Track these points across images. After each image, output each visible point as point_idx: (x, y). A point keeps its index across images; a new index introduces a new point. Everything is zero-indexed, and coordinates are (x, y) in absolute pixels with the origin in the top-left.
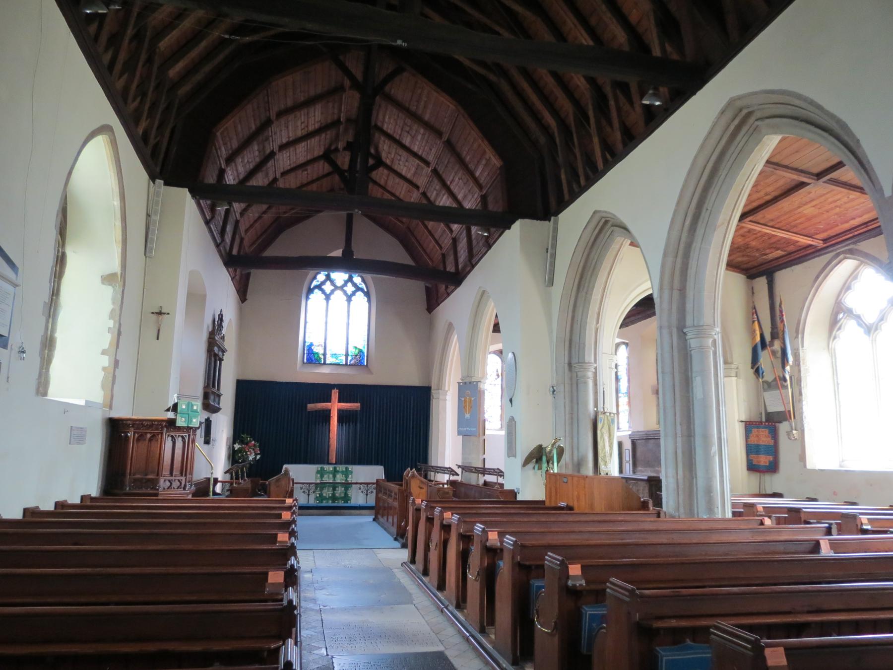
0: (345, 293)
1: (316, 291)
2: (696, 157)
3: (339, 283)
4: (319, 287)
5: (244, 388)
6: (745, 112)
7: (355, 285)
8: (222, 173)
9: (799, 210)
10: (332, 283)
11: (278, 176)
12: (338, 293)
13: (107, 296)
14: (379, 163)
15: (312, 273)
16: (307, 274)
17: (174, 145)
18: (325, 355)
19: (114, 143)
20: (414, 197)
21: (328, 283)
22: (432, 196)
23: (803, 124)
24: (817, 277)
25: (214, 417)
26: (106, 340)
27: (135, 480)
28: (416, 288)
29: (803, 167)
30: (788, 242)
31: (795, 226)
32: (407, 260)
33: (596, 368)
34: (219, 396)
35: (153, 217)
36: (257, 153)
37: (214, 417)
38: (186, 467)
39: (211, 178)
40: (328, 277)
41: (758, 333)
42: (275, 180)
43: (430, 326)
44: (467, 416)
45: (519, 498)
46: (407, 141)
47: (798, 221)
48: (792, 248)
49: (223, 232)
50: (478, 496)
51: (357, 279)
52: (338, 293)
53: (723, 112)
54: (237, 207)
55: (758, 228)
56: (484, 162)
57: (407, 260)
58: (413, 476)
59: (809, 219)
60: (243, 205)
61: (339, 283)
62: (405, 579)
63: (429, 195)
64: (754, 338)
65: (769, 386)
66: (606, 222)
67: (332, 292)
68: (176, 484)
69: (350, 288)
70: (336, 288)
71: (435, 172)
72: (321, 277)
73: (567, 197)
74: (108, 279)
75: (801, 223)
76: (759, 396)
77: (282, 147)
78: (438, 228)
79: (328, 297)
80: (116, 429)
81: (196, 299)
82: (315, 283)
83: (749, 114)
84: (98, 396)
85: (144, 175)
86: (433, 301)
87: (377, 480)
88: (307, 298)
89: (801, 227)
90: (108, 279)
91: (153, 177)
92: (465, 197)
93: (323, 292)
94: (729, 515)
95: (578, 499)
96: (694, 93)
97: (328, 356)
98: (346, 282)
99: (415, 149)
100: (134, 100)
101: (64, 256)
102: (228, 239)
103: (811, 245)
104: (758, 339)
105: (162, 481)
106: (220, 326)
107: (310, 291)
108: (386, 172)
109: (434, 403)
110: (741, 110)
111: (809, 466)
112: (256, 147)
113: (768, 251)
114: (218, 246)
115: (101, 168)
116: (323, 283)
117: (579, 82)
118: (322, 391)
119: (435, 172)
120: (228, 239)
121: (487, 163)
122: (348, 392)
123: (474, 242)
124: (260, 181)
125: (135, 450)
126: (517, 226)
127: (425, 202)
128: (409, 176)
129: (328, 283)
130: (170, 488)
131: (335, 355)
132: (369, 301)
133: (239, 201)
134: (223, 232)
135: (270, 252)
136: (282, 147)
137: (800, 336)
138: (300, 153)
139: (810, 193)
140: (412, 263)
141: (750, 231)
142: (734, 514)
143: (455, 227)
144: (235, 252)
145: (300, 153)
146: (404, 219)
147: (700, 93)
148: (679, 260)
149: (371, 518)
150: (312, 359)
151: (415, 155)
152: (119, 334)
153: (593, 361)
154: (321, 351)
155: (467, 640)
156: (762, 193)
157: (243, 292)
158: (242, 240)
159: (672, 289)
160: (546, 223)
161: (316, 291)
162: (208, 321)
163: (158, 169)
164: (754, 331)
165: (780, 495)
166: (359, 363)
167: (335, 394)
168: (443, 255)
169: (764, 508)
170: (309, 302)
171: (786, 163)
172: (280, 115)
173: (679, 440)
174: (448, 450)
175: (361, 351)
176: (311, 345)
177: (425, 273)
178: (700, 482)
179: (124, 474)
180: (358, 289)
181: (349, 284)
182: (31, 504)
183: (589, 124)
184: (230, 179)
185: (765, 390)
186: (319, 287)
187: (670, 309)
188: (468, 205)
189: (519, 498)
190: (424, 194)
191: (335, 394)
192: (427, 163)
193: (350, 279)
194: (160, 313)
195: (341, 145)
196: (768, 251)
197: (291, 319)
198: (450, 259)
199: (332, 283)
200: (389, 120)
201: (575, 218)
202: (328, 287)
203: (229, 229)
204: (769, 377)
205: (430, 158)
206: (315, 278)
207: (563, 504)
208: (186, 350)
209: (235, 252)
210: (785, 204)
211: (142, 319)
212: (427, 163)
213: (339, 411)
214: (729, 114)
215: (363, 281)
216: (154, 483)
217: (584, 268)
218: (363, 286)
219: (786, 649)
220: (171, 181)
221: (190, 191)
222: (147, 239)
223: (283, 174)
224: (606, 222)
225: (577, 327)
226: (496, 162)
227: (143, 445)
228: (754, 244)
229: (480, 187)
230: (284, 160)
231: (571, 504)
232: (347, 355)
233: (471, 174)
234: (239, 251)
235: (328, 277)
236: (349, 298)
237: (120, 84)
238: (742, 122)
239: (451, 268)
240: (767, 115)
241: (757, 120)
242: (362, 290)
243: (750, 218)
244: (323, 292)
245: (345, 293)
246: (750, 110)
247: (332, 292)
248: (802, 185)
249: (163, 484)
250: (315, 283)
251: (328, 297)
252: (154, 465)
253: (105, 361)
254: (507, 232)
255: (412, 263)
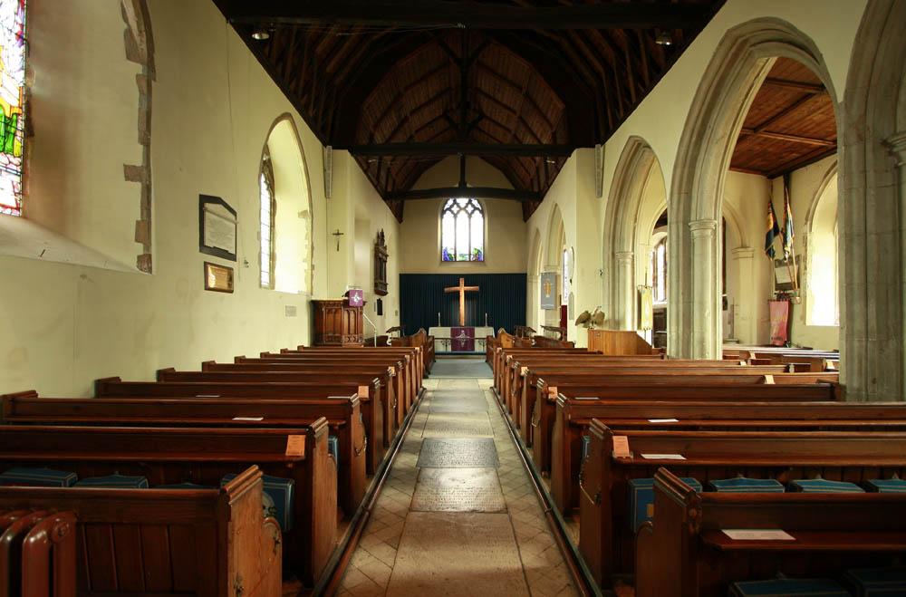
0: (467, 212)
1: (448, 212)
2: (700, 84)
3: (463, 205)
4: (449, 209)
5: (405, 280)
6: (740, 41)
7: (473, 206)
8: (372, 137)
9: (809, 118)
10: (458, 206)
11: (413, 133)
12: (463, 212)
13: (303, 225)
14: (482, 116)
15: (444, 199)
16: (440, 201)
17: (334, 123)
18: (455, 255)
19: (293, 124)
20: (508, 140)
21: (455, 206)
22: (520, 136)
23: (786, 45)
24: (828, 173)
25: (383, 298)
26: (306, 252)
27: (329, 337)
28: (515, 206)
29: (807, 81)
30: (802, 145)
31: (806, 132)
32: (510, 187)
33: (633, 256)
34: (386, 285)
35: (327, 172)
36: (395, 119)
37: (383, 298)
38: (358, 328)
39: (365, 142)
40: (455, 202)
41: (772, 222)
42: (411, 137)
43: (527, 231)
44: (548, 296)
45: (576, 346)
46: (499, 97)
47: (809, 127)
48: (805, 150)
49: (378, 179)
50: (556, 345)
51: (475, 202)
52: (463, 212)
53: (721, 44)
54: (388, 159)
55: (771, 137)
56: (552, 106)
57: (510, 187)
58: (503, 333)
59: (818, 125)
60: (391, 157)
61: (463, 205)
62: (489, 397)
63: (518, 135)
64: (768, 223)
65: (780, 263)
66: (639, 144)
67: (458, 212)
68: (352, 339)
69: (470, 209)
70: (461, 209)
71: (520, 118)
72: (450, 202)
73: (611, 127)
74: (303, 214)
75: (813, 128)
76: (770, 271)
77: (412, 113)
78: (526, 160)
79: (455, 216)
80: (316, 307)
81: (359, 224)
82: (447, 207)
83: (746, 41)
84: (304, 288)
85: (319, 143)
86: (527, 213)
87: (488, 337)
88: (442, 217)
89: (812, 131)
90: (303, 214)
91: (325, 144)
92: (542, 135)
93: (452, 212)
94: (721, 358)
95: (606, 346)
96: (701, 30)
97: (457, 255)
98: (467, 204)
99: (505, 102)
100: (303, 96)
101: (274, 200)
102: (383, 182)
103: (822, 147)
104: (772, 226)
105: (343, 337)
106: (383, 240)
107: (444, 212)
108: (488, 122)
109: (529, 284)
110: (736, 40)
111: (808, 324)
112: (393, 116)
113: (784, 155)
114: (376, 187)
115: (288, 143)
116: (452, 206)
117: (619, 33)
118: (453, 279)
119: (520, 118)
120: (383, 182)
121: (554, 106)
122: (470, 279)
123: (549, 168)
124: (400, 138)
125: (328, 319)
126: (575, 153)
127: (516, 142)
128: (503, 124)
129: (455, 206)
130: (349, 343)
131: (462, 255)
132: (483, 216)
133: (388, 155)
134: (378, 179)
135: (415, 188)
136: (412, 113)
137: (809, 223)
138: (426, 116)
139: (817, 102)
140: (513, 188)
141: (766, 139)
142: (724, 357)
143: (537, 159)
144: (389, 189)
145: (426, 116)
146: (503, 157)
147: (705, 30)
148: (686, 170)
149: (484, 361)
150: (449, 259)
151: (506, 107)
152: (313, 248)
153: (630, 250)
154: (452, 253)
155: (510, 432)
156: (773, 107)
157: (399, 216)
158: (394, 181)
159: (680, 193)
160: (591, 149)
161: (448, 212)
162: (375, 236)
163: (328, 139)
164: (769, 220)
165: (811, 349)
166: (478, 260)
167: (462, 281)
168: (532, 180)
169: (756, 354)
170: (444, 220)
171: (791, 78)
172: (407, 89)
173: (681, 305)
174: (539, 319)
175: (479, 251)
176: (446, 250)
177: (519, 196)
178: (696, 335)
179: (322, 333)
180: (476, 209)
181: (470, 206)
182: (265, 351)
183: (626, 64)
184: (379, 139)
185: (776, 267)
186: (449, 209)
187: (678, 209)
188: (545, 142)
189: (576, 346)
190: (515, 136)
191: (462, 281)
192: (514, 112)
193: (470, 202)
194: (338, 234)
195: (454, 106)
196: (784, 155)
197: (432, 233)
198: (535, 183)
199: (458, 206)
200: (485, 83)
201: (616, 146)
202: (455, 209)
203: (383, 173)
204: (779, 256)
205: (516, 108)
206: (446, 203)
207: (596, 350)
208: (362, 255)
209: (389, 189)
210: (796, 114)
211: (328, 238)
212: (514, 112)
213: (465, 291)
214: (727, 43)
215: (479, 202)
216: (339, 339)
217: (625, 177)
218: (479, 206)
219: (628, 438)
220: (338, 146)
221: (349, 151)
222: (325, 186)
223: (417, 131)
224: (639, 144)
225: (618, 226)
226: (561, 106)
227: (331, 316)
228: (771, 149)
229: (551, 126)
230: (416, 122)
231: (601, 350)
232: (470, 255)
233: (545, 117)
234: (393, 189)
235: (455, 202)
236: (470, 216)
237: (292, 87)
238: (738, 48)
239: (536, 190)
240: (758, 41)
241: (751, 46)
242: (478, 209)
243: (764, 129)
244: (452, 212)
245: (467, 212)
246: (744, 38)
247: (458, 212)
248: (808, 96)
249: (344, 338)
250: (447, 207)
251: (455, 216)
252: (338, 328)
253: (306, 266)
254: (569, 159)
255: (513, 188)
